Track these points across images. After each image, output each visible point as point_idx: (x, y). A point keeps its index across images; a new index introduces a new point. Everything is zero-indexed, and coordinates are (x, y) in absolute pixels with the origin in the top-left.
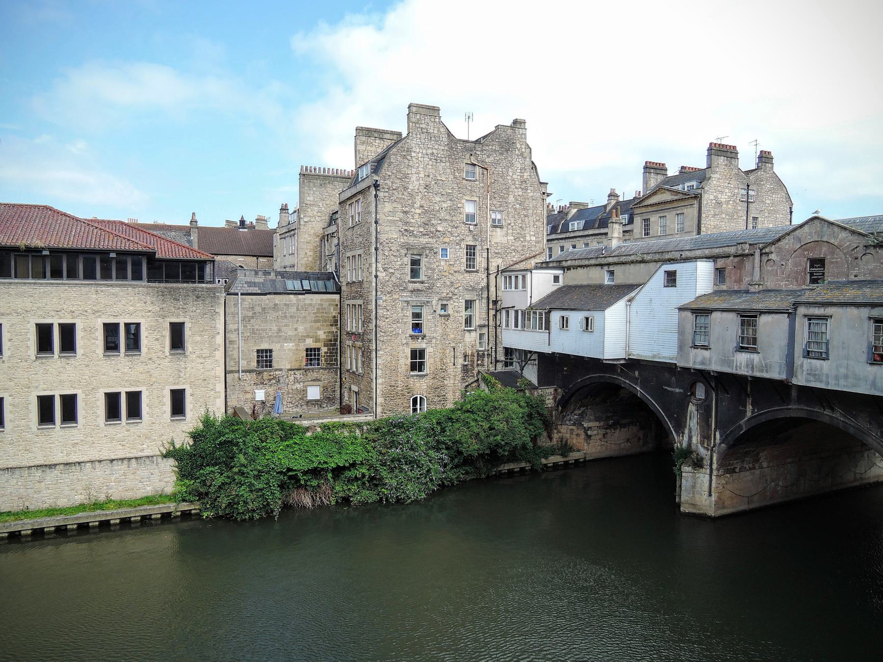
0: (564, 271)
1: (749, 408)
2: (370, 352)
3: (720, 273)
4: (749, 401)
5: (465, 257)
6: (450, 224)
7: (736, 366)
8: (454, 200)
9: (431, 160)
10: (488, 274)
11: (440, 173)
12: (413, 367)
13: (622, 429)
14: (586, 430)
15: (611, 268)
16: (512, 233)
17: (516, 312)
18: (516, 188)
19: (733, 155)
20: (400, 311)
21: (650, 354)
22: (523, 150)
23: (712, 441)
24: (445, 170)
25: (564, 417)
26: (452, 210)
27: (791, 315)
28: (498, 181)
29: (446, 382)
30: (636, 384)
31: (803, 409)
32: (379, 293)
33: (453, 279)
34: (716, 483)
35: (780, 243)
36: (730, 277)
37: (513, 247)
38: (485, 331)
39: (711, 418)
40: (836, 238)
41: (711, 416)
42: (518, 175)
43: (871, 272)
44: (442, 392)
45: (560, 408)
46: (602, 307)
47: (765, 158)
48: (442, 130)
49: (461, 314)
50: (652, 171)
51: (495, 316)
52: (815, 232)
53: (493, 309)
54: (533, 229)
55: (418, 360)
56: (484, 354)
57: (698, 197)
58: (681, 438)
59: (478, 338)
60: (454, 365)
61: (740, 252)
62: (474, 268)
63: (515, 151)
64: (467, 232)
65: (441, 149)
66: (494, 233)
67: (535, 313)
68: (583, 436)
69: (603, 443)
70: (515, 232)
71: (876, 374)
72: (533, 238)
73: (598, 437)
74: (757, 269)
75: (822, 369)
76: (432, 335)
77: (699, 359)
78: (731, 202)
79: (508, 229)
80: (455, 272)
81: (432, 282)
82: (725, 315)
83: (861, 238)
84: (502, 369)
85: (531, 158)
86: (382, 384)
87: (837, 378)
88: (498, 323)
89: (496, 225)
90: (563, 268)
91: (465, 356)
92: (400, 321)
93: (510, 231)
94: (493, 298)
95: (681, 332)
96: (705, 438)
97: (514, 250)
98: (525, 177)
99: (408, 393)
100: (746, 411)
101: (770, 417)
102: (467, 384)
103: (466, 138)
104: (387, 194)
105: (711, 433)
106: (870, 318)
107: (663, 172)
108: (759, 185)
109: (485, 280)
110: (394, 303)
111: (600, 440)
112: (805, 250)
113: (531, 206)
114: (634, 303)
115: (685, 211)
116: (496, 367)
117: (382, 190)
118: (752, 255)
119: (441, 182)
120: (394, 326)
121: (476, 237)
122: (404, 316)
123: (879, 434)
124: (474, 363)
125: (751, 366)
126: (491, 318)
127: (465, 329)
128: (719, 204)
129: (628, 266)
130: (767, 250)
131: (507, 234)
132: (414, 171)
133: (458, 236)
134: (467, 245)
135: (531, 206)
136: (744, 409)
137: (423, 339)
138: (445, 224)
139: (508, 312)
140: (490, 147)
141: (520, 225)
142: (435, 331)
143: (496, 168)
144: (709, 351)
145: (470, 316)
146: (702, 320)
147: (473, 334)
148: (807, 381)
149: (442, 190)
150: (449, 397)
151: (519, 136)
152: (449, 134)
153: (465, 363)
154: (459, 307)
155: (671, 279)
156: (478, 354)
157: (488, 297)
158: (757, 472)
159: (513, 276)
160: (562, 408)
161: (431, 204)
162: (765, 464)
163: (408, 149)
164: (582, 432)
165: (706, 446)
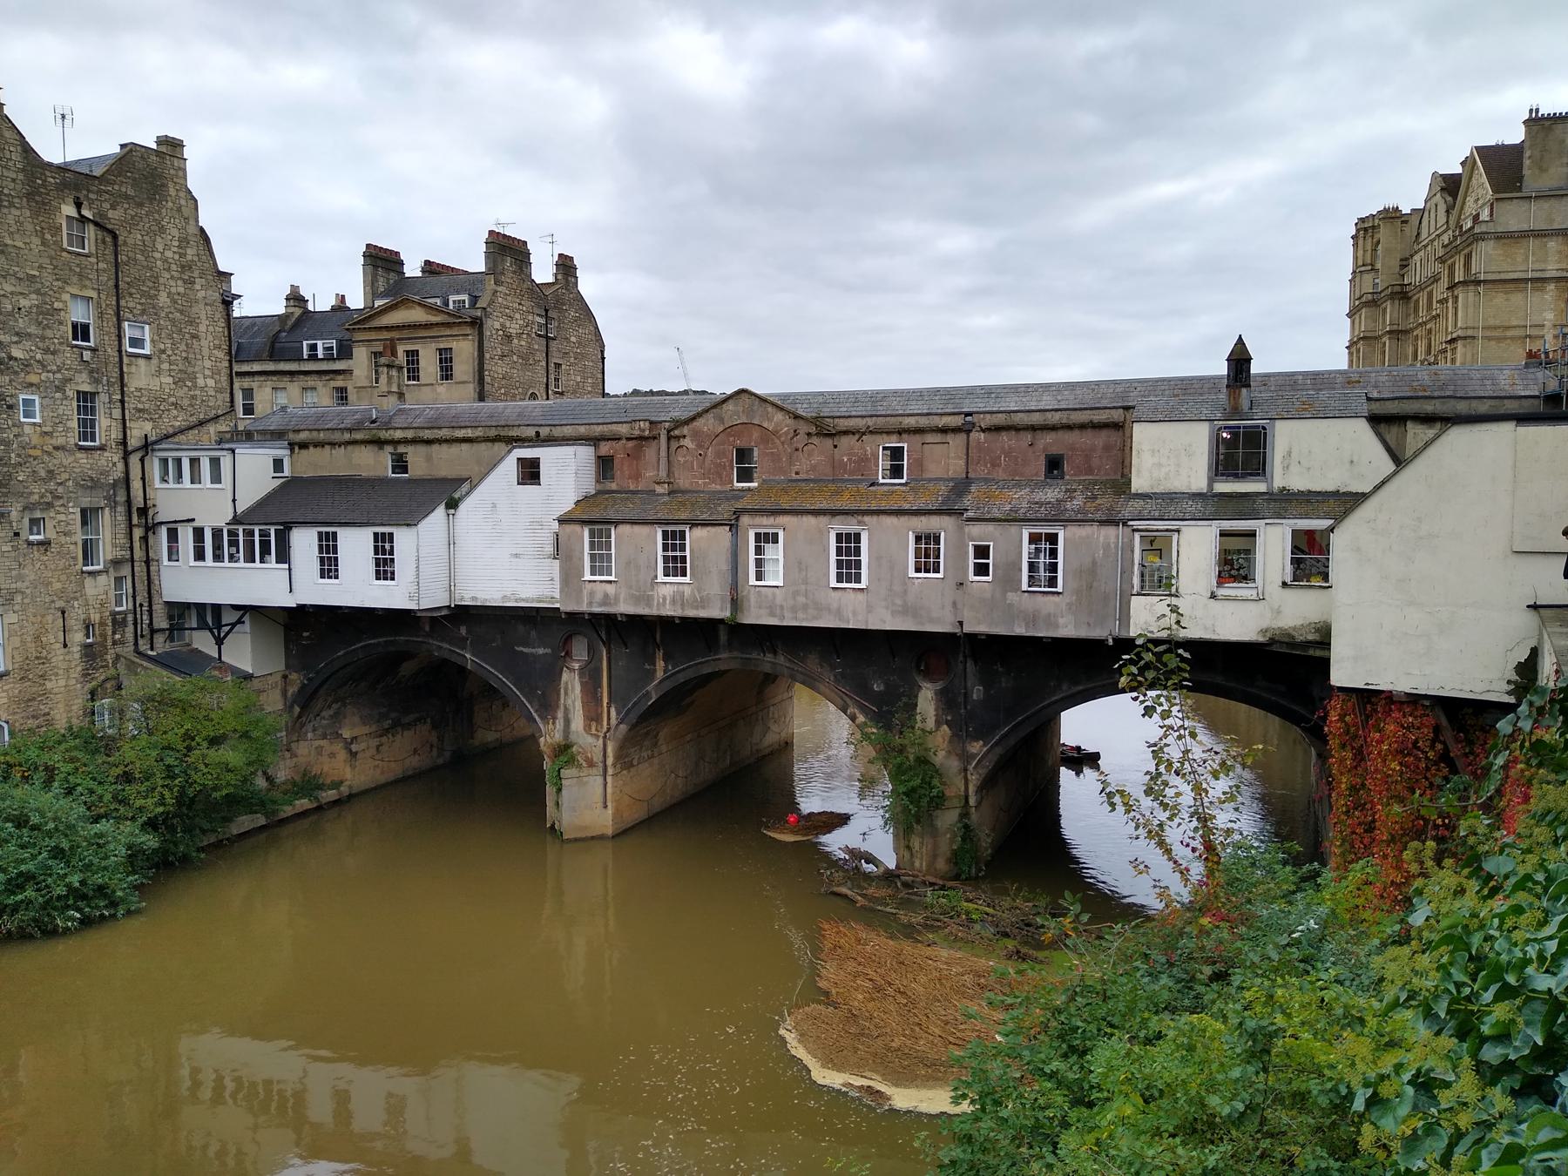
0: (292, 450)
1: (660, 664)
3: (605, 465)
5: (76, 417)
6: (40, 345)
8: (45, 294)
11: (11, 229)
13: (406, 733)
14: (348, 744)
16: (170, 370)
18: (172, 277)
22: (183, 202)
23: (605, 723)
24: (22, 224)
25: (303, 725)
26: (42, 313)
27: (733, 527)
28: (135, 260)
29: (49, 685)
34: (614, 787)
37: (172, 400)
38: (126, 571)
41: (600, 686)
42: (174, 252)
43: (814, 468)
44: (42, 707)
45: (297, 709)
46: (410, 520)
47: (566, 266)
49: (74, 539)
51: (145, 539)
53: (138, 526)
54: (208, 364)
56: (124, 619)
57: (477, 324)
58: (551, 726)
60: (65, 646)
61: (637, 433)
62: (93, 440)
63: (167, 201)
66: (133, 369)
68: (342, 755)
69: (377, 763)
70: (174, 367)
72: (211, 382)
73: (368, 754)
74: (663, 461)
76: (14, 586)
77: (599, 597)
78: (525, 336)
79: (161, 362)
80: (56, 448)
82: (637, 529)
84: (164, 647)
85: (197, 221)
87: (794, 610)
91: (87, 628)
93: (165, 366)
94: (138, 501)
97: (175, 405)
98: (189, 258)
100: (655, 670)
101: (690, 674)
102: (94, 683)
105: (602, 712)
107: (397, 267)
108: (561, 311)
109: (120, 466)
111: (372, 757)
112: (730, 435)
118: (655, 438)
123: (832, 678)
124: (106, 640)
126: (137, 544)
127: (85, 568)
128: (509, 337)
129: (436, 447)
130: (677, 432)
131: (159, 372)
133: (59, 371)
134: (78, 392)
138: (27, 344)
139: (173, 535)
140: (116, 187)
141: (184, 355)
142: (20, 578)
147: (102, 579)
149: (17, 269)
150: (58, 717)
151: (172, 172)
153: (88, 641)
154: (69, 524)
155: (530, 473)
156: (114, 622)
158: (656, 761)
159: (170, 460)
160: (302, 708)
164: (338, 747)
165: (594, 732)
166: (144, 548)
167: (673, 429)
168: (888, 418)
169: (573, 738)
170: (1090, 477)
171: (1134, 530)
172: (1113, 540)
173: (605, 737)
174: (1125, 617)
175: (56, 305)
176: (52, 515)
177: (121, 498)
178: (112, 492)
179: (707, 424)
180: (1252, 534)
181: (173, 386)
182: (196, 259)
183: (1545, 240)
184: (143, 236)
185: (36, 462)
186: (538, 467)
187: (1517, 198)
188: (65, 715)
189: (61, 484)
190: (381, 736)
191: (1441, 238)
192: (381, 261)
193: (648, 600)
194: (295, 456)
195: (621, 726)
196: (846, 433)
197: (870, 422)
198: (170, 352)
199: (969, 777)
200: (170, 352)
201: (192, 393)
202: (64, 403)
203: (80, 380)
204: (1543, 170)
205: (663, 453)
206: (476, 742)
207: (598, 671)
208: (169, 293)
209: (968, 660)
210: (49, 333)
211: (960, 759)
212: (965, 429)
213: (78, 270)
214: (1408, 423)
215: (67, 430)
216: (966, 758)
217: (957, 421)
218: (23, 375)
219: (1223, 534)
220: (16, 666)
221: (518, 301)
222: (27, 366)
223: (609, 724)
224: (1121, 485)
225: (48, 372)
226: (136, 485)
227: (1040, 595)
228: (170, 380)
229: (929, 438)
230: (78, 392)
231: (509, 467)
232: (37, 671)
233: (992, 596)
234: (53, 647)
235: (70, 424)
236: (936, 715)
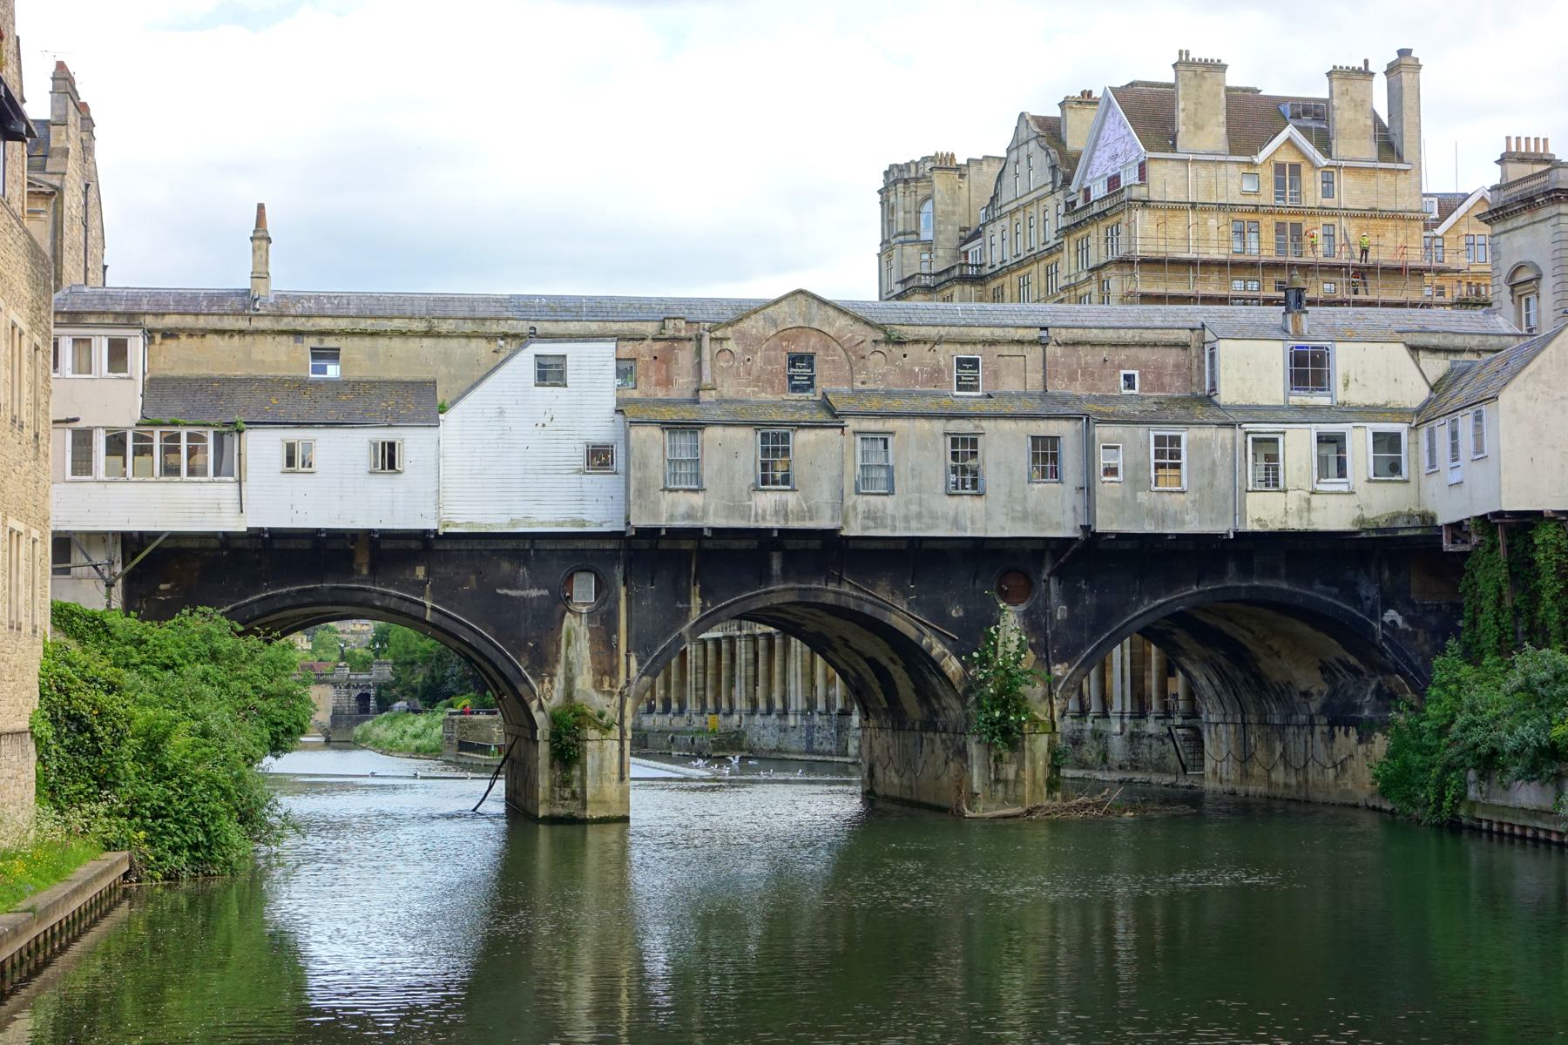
0: (151, 340)
1: (696, 602)
3: (625, 369)
4: (696, 590)
7: (756, 515)
21: (505, 519)
31: (792, 589)
36: (647, 376)
39: (616, 633)
40: (831, 325)
41: (616, 631)
52: (800, 314)
58: (547, 685)
71: (957, 508)
75: (885, 509)
77: (682, 509)
82: (731, 431)
83: (869, 329)
87: (907, 519)
96: (604, 673)
100: (689, 609)
103: (1455, 192)
106: (946, 434)
112: (782, 339)
125: (783, 513)
136: (685, 605)
144: (701, 494)
148: (865, 528)
170: (1163, 394)
171: (1247, 433)
172: (1229, 442)
174: (1239, 511)
179: (754, 326)
183: (1205, 216)
187: (1172, 159)
191: (1029, 209)
194: (154, 348)
195: (644, 678)
196: (916, 342)
197: (943, 331)
204: (1199, 127)
214: (1420, 353)
217: (1035, 334)
223: (628, 675)
224: (1208, 400)
227: (1166, 494)
229: (1005, 350)
231: (524, 362)
233: (1123, 496)
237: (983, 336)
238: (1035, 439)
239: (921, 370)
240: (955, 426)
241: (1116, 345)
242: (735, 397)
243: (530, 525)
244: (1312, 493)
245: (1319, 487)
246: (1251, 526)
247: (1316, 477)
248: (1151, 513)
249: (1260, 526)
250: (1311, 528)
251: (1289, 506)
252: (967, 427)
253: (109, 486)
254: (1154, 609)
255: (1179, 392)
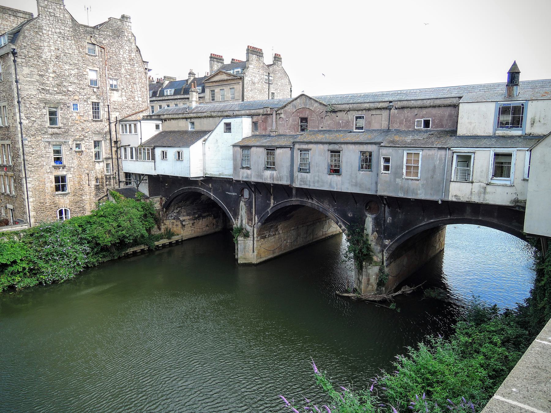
0: (162, 121)
1: (272, 201)
2: (21, 180)
3: (255, 124)
4: (272, 197)
6: (79, 86)
9: (59, 37)
10: (110, 123)
12: (57, 189)
14: (182, 222)
15: (193, 121)
16: (125, 95)
17: (132, 149)
19: (261, 55)
20: (43, 149)
21: (218, 173)
22: (130, 37)
24: (71, 46)
25: (167, 215)
26: (79, 76)
30: (210, 192)
31: (298, 200)
32: (24, 136)
33: (83, 126)
34: (257, 245)
35: (286, 108)
37: (126, 105)
38: (110, 161)
40: (313, 106)
42: (127, 55)
43: (329, 125)
44: (82, 205)
45: (165, 210)
46: (188, 144)
47: (277, 58)
48: (66, 15)
50: (215, 60)
51: (117, 151)
52: (303, 103)
53: (114, 147)
54: (139, 93)
55: (61, 184)
56: (110, 178)
57: (242, 79)
59: (105, 166)
60: (89, 185)
61: (265, 113)
62: (99, 118)
64: (91, 93)
65: (67, 30)
66: (112, 94)
67: (144, 149)
68: (180, 225)
69: (192, 229)
70: (127, 94)
72: (140, 99)
73: (189, 225)
74: (274, 123)
75: (307, 178)
76: (70, 165)
77: (245, 175)
80: (85, 121)
81: (67, 128)
82: (258, 149)
85: (135, 44)
86: (33, 202)
87: (314, 182)
88: (119, 156)
89: (113, 89)
90: (162, 120)
91: (97, 179)
92: (44, 156)
93: (124, 94)
94: (114, 139)
95: (235, 159)
97: (128, 107)
98: (132, 57)
99: (55, 207)
100: (270, 203)
101: (283, 206)
102: (99, 198)
104: (24, 61)
108: (274, 74)
109: (108, 127)
110: (37, 143)
111: (191, 227)
112: (298, 112)
113: (138, 77)
114: (207, 142)
115: (235, 87)
116: (119, 186)
117: (19, 57)
118: (272, 114)
119: (68, 54)
120: (40, 160)
121: (98, 96)
122: (47, 152)
123: (333, 210)
126: (114, 153)
128: (254, 83)
129: (202, 119)
130: (279, 112)
132: (46, 44)
133: (85, 95)
135: (138, 77)
137: (63, 168)
138: (74, 86)
139: (125, 149)
141: (131, 90)
143: (111, 48)
144: (250, 170)
145: (99, 152)
146: (246, 152)
147: (102, 164)
148: (300, 185)
150: (87, 208)
151: (126, 27)
152: (73, 20)
153: (97, 184)
154: (89, 146)
155: (228, 127)
156: (106, 178)
157: (111, 139)
159: (127, 125)
161: (62, 70)
162: (281, 232)
163: (39, 26)
164: (179, 223)
166: (116, 154)
167: (278, 110)
168: (358, 104)
169: (244, 226)
170: (442, 129)
171: (453, 153)
172: (443, 156)
173: (254, 227)
174: (447, 191)
175: (84, 73)
176: (84, 142)
177: (108, 137)
178: (105, 135)
179: (289, 108)
180: (510, 155)
181: (127, 100)
182: (135, 57)
184: (115, 49)
185: (78, 125)
186: (230, 126)
188: (89, 207)
189: (87, 132)
190: (194, 220)
192: (215, 58)
193: (261, 178)
194: (163, 123)
196: (341, 111)
197: (351, 106)
198: (125, 89)
199: (384, 254)
200: (125, 89)
201: (134, 103)
202: (88, 105)
203: (93, 98)
205: (274, 120)
206: (375, 215)
207: (251, 202)
208: (125, 69)
209: (386, 206)
210: (81, 82)
211: (381, 247)
212: (389, 109)
213: (92, 61)
215: (88, 115)
216: (383, 246)
218: (72, 96)
219: (497, 155)
220: (72, 191)
221: (258, 70)
222: (74, 93)
223: (255, 222)
224: (453, 132)
225: (82, 95)
226: (113, 133)
228: (126, 98)
229: (374, 112)
230: (93, 102)
232: (79, 193)
234: (85, 185)
235: (89, 113)
236: (373, 228)
237: (366, 107)
238: (363, 153)
239: (342, 122)
240: (332, 147)
241: (421, 107)
242: (283, 134)
243: (223, 175)
244: (487, 184)
245: (493, 182)
246: (451, 198)
247: (491, 176)
248: (402, 188)
249: (456, 199)
250: (484, 202)
251: (473, 190)
252: (336, 147)
253: (136, 162)
254: (429, 223)
255: (450, 128)
